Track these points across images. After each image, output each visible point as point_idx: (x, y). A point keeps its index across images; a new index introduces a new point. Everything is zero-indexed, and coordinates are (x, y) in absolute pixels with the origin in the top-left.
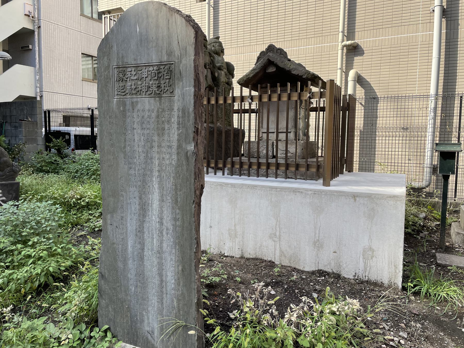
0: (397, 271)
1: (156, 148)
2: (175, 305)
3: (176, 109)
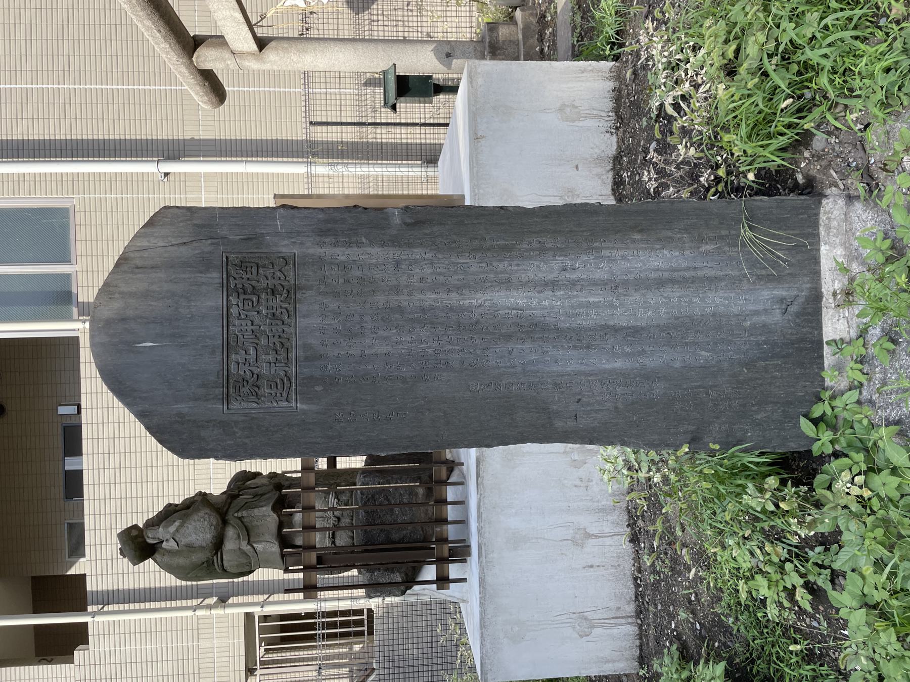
0: (590, 68)
1: (402, 297)
2: (713, 247)
3: (319, 251)
